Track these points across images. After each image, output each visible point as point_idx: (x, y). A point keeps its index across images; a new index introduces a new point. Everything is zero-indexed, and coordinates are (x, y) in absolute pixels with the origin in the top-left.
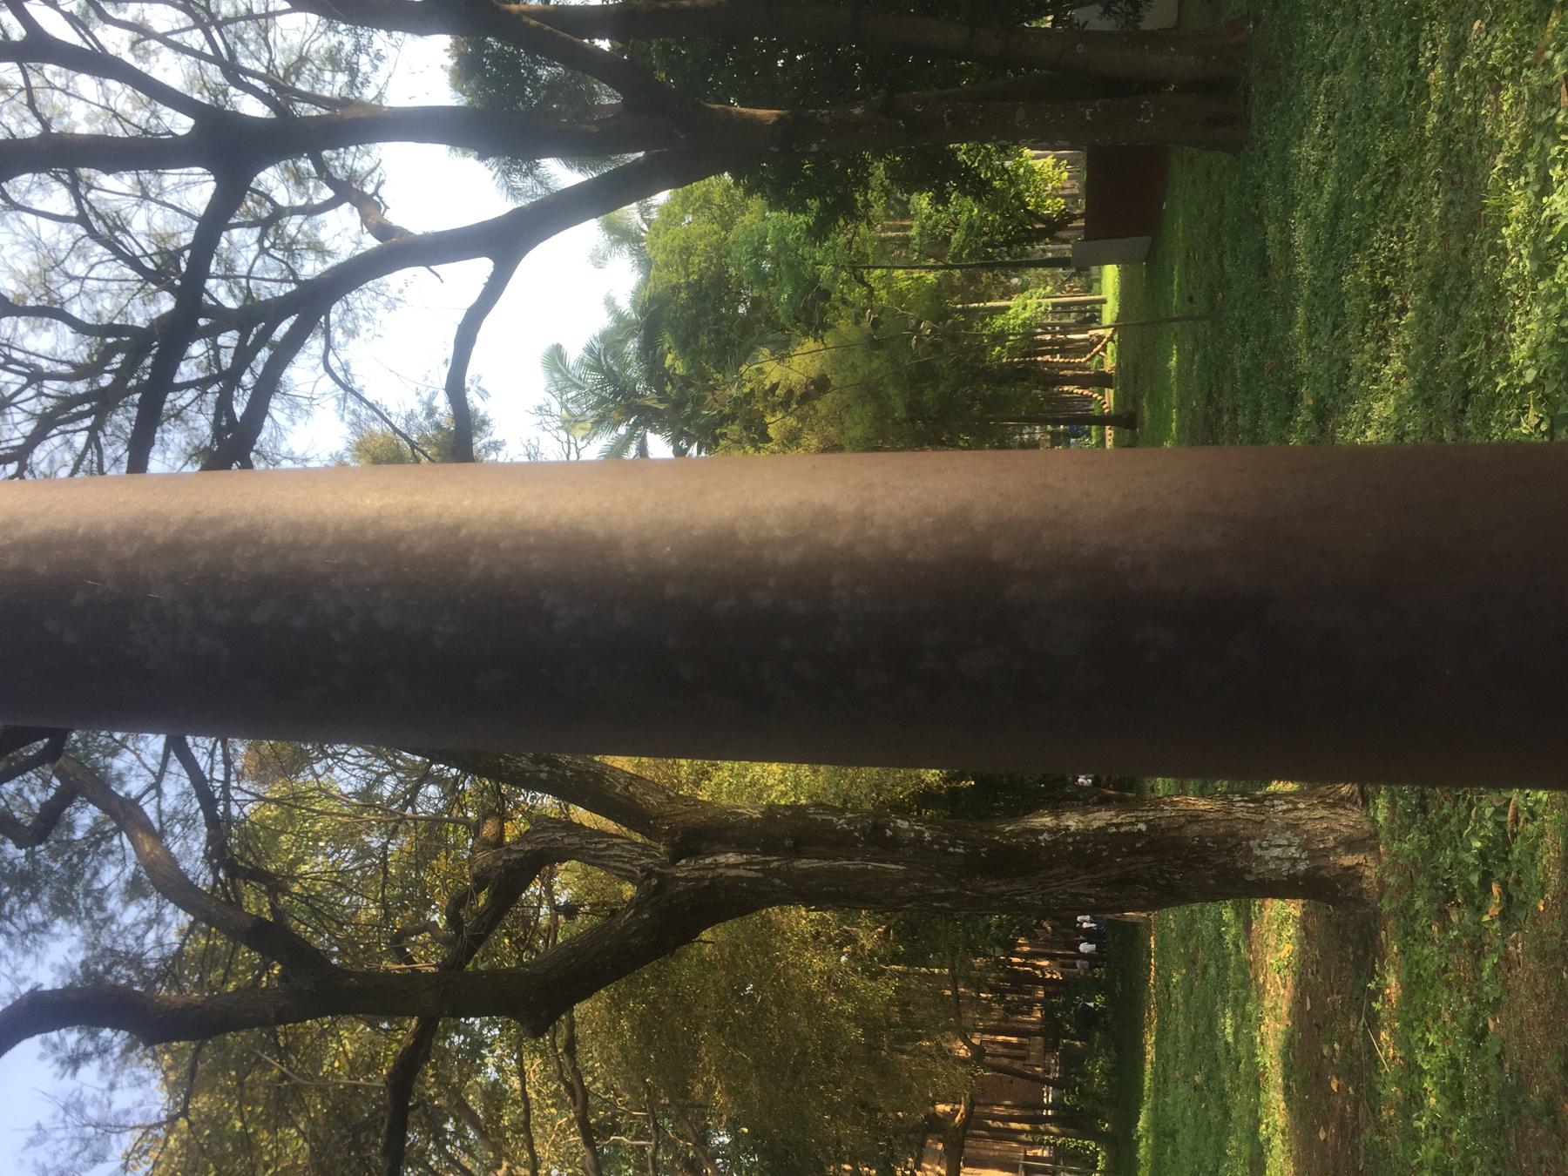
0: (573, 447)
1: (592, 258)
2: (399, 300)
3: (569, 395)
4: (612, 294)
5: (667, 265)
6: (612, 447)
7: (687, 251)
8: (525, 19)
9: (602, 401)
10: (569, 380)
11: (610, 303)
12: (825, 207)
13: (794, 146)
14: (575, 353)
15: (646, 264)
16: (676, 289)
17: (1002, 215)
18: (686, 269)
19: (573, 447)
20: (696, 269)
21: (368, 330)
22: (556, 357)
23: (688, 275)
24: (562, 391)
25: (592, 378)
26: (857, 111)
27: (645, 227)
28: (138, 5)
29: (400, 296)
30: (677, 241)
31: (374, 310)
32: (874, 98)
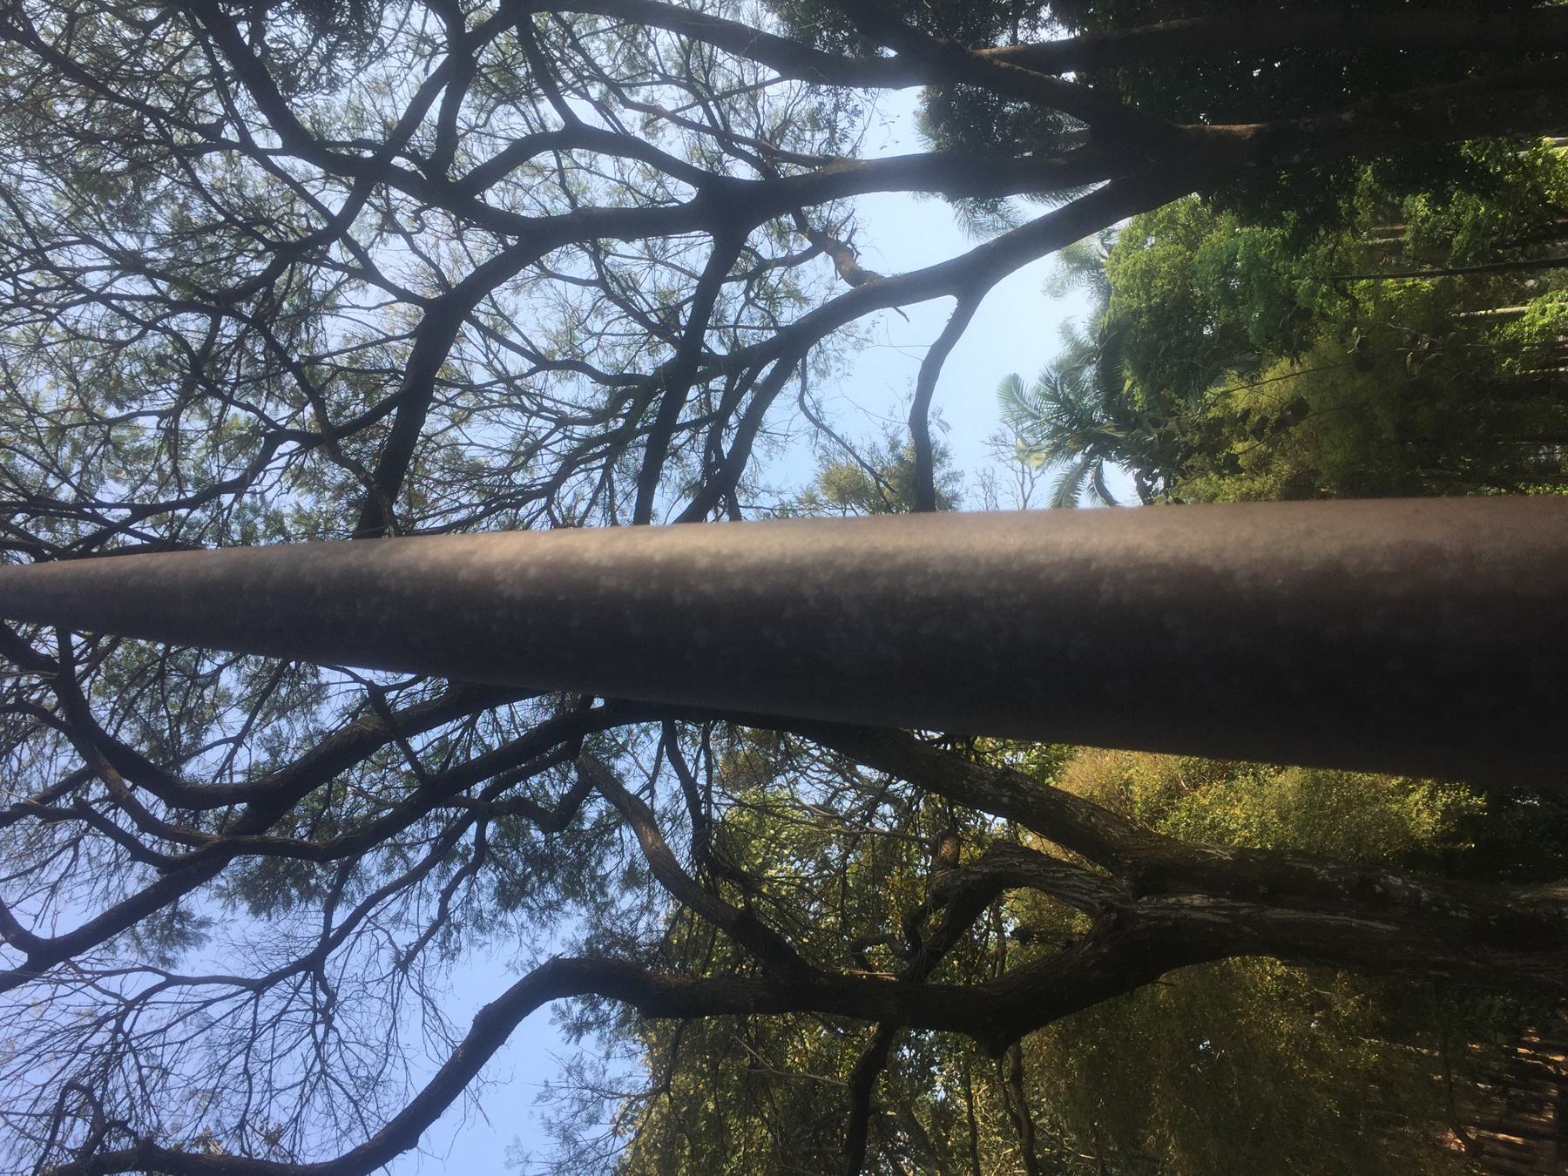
0: (1027, 476)
2: (866, 340)
3: (1025, 425)
4: (1070, 322)
5: (1127, 290)
6: (1067, 476)
7: (1149, 273)
8: (996, 62)
9: (1058, 430)
10: (1025, 409)
11: (1067, 330)
14: (1032, 381)
15: (1106, 290)
16: (1137, 314)
17: (1515, 212)
18: (1148, 293)
19: (1027, 476)
20: (1158, 292)
22: (1013, 387)
23: (1149, 299)
24: (1018, 421)
25: (1049, 407)
26: (1346, 116)
27: (1105, 253)
29: (868, 337)
30: (1138, 265)
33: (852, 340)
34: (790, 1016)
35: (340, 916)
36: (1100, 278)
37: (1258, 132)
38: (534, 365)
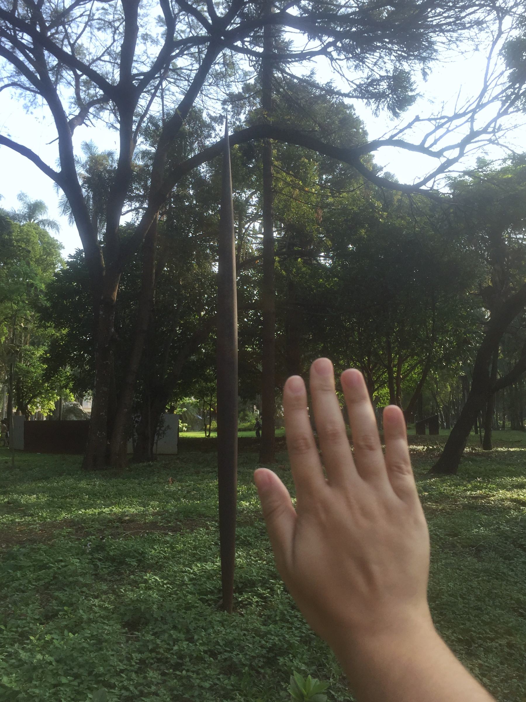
1: (23, 194)
2: (28, 111)
5: (22, 231)
7: (28, 241)
12: (47, 308)
13: (103, 305)
15: (15, 217)
16: (10, 234)
21: (15, 93)
23: (17, 241)
26: (113, 330)
27: (36, 221)
28: (163, 45)
29: (29, 112)
30: (33, 238)
31: (25, 99)
32: (117, 336)
33: (29, 104)
34: (192, 81)
35: (493, 125)
36: (24, 217)
37: (113, 301)
38: (430, 149)
